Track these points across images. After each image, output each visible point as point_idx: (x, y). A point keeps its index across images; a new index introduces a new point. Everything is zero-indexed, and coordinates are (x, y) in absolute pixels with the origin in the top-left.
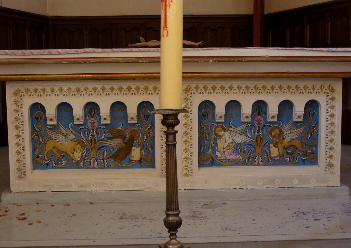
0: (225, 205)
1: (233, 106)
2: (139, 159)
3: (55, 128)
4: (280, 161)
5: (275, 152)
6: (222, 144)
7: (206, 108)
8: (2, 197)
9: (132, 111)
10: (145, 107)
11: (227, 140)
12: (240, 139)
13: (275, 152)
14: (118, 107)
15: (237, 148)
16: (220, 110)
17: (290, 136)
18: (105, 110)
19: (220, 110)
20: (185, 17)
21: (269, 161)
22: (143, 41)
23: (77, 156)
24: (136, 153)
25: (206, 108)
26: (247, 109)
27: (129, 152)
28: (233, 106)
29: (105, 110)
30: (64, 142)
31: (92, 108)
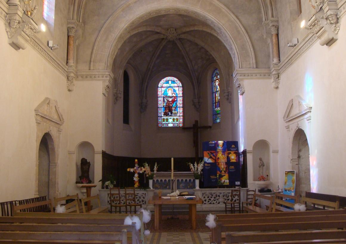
0: (60, 113)
1: (182, 180)
2: (197, 210)
3: (156, 183)
4: (190, 188)
5: (189, 187)
6: (181, 186)
7: (178, 180)
8: (168, 78)
9: (167, 180)
10: (169, 180)
11: (181, 185)
12: (183, 185)
13: (189, 187)
14: (165, 180)
15: (183, 186)
16: (180, 181)
17: (191, 185)
18: (163, 181)
19: (180, 181)
20: (170, 171)
21: (188, 188)
22: (136, 177)
23: (159, 187)
24: (168, 187)
25: (178, 180)
26: (184, 181)
27: (167, 187)
28: (182, 180)
29: (163, 181)
30: (157, 185)
31: (161, 180)
